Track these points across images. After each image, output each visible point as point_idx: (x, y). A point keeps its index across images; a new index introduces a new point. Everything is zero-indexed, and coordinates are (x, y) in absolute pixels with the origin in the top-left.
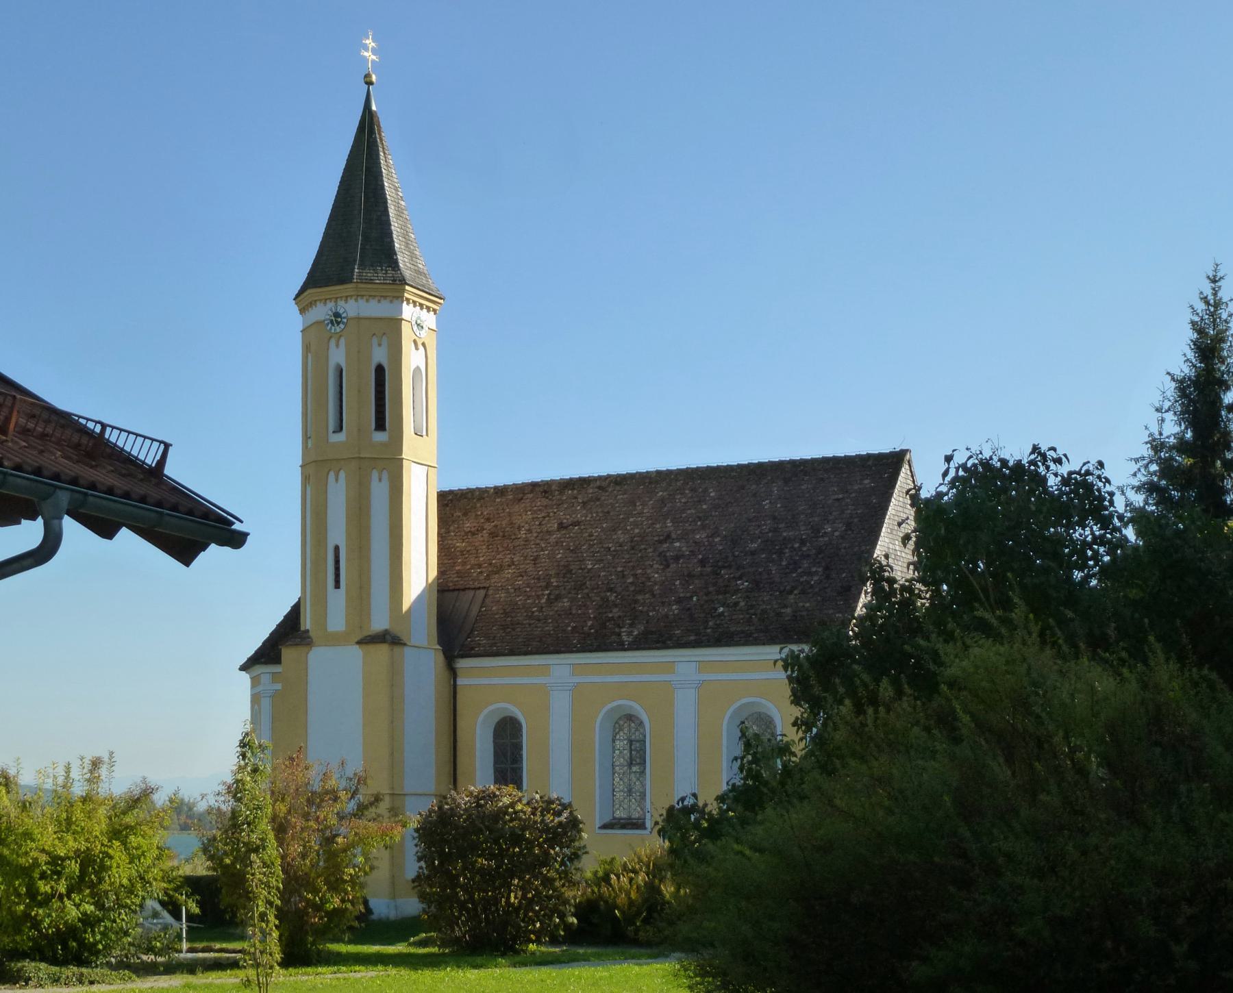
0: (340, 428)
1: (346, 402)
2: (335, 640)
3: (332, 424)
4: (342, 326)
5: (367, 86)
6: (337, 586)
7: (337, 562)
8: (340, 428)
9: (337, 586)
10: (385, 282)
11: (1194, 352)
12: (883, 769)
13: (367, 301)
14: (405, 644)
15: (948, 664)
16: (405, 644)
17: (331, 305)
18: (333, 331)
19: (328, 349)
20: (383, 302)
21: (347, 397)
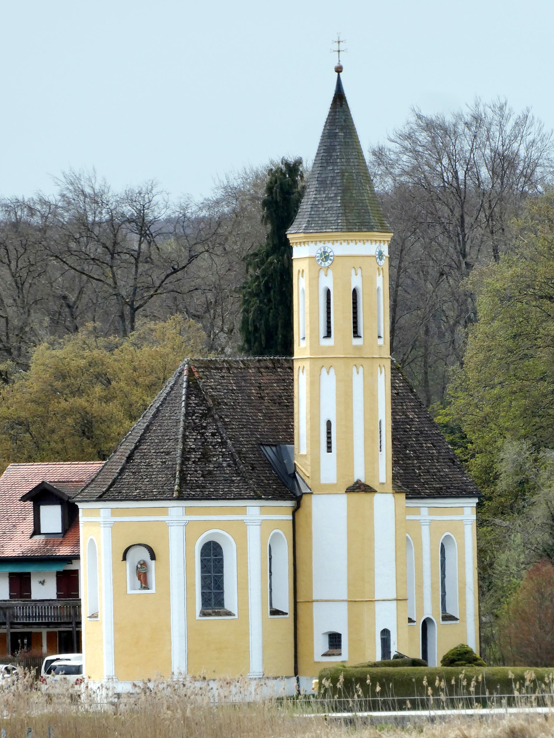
0: (328, 334)
1: (334, 310)
2: (329, 490)
3: (323, 331)
4: (330, 262)
5: (337, 73)
6: (329, 449)
7: (329, 433)
8: (328, 334)
9: (329, 449)
10: (321, 231)
11: (6, 223)
12: (526, 188)
13: (348, 243)
14: (375, 491)
15: (508, 197)
16: (375, 491)
17: (321, 245)
18: (323, 265)
19: (318, 277)
20: (359, 244)
21: (334, 305)
